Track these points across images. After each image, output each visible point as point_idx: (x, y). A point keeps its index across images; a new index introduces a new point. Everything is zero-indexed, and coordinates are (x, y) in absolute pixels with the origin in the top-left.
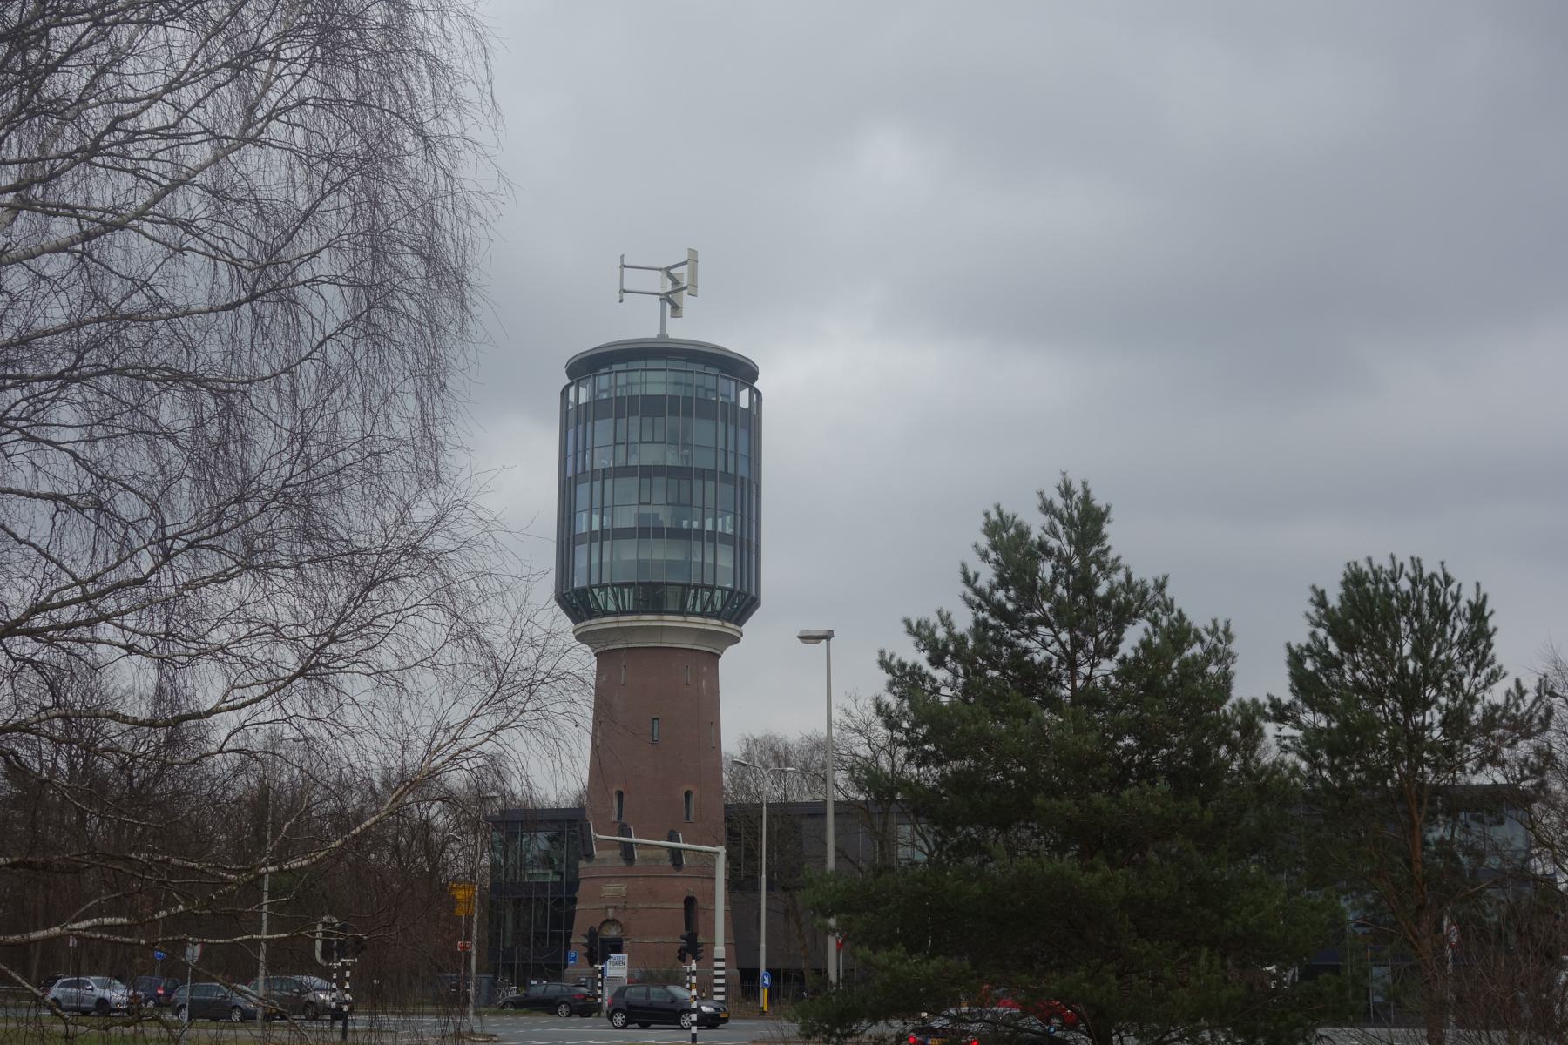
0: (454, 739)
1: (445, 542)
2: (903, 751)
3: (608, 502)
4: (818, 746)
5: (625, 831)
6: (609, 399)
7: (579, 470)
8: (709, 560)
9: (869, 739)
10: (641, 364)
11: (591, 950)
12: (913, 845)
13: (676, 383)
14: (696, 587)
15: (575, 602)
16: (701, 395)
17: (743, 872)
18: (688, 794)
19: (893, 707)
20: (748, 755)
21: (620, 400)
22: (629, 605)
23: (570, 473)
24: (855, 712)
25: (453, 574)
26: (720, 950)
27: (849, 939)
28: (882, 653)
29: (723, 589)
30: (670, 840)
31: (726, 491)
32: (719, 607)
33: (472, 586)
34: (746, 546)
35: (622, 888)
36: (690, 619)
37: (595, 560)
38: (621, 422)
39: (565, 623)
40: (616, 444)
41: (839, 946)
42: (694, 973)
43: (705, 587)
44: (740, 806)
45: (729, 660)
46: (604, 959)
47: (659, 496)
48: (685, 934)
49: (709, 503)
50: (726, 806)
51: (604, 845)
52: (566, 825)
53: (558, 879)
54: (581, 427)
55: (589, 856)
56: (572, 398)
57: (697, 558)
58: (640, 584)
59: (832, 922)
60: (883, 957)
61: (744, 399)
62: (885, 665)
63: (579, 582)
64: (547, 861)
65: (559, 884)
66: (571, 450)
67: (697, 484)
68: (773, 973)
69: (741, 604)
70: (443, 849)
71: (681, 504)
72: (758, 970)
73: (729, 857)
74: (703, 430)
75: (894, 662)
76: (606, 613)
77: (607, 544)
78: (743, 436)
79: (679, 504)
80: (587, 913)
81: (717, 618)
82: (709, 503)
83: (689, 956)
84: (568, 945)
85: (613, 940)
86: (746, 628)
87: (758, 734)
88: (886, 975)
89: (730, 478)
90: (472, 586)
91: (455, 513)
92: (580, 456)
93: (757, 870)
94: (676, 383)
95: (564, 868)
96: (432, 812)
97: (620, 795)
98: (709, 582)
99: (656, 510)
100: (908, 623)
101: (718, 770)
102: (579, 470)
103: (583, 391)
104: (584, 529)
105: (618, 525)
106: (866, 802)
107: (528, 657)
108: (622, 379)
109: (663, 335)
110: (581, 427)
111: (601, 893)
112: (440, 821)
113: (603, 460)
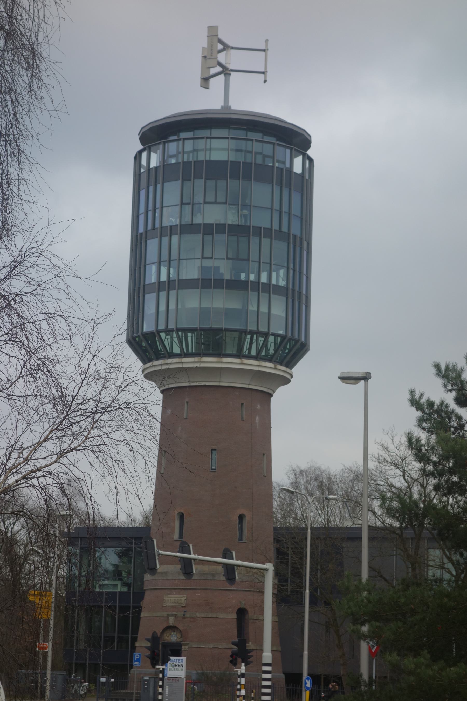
0: (26, 460)
1: (23, 284)
2: (433, 481)
3: (174, 255)
4: (357, 477)
5: (184, 548)
6: (177, 163)
7: (150, 227)
8: (264, 309)
9: (404, 472)
10: (206, 133)
11: (153, 652)
12: (442, 567)
13: (237, 150)
14: (252, 333)
15: (145, 345)
16: (259, 160)
17: (289, 588)
18: (241, 517)
19: (423, 442)
20: (295, 484)
21: (186, 164)
22: (192, 348)
23: (141, 229)
24: (391, 447)
25: (27, 315)
26: (267, 656)
27: (383, 648)
28: (412, 392)
29: (276, 335)
30: (225, 557)
31: (280, 247)
32: (272, 351)
33: (44, 325)
34: (297, 297)
35: (181, 599)
36: (246, 361)
37: (162, 308)
38: (188, 184)
39: (133, 364)
40: (182, 204)
41: (372, 655)
42: (243, 675)
43: (258, 333)
44: (288, 529)
45: (281, 399)
46: (165, 661)
47: (220, 252)
48: (236, 640)
49: (265, 258)
50: (275, 529)
51: (166, 560)
52: (133, 542)
53: (125, 589)
54: (151, 189)
55: (153, 570)
56: (144, 162)
57: (253, 307)
58: (201, 329)
59: (365, 629)
60: (409, 662)
61: (298, 166)
62: (415, 403)
63: (148, 326)
64: (117, 573)
65: (128, 593)
66: (142, 209)
67: (254, 241)
68: (315, 678)
69: (292, 349)
70: (25, 560)
71: (239, 259)
72: (301, 675)
73: (277, 574)
74: (261, 193)
75: (423, 400)
76: (171, 355)
77: (173, 293)
78: (296, 198)
79: (237, 259)
80: (151, 619)
81: (270, 361)
82: (265, 258)
83: (239, 660)
84: (134, 648)
85: (173, 644)
86: (297, 370)
87: (304, 466)
88: (412, 678)
89: (284, 236)
90: (44, 325)
91: (32, 259)
92: (150, 214)
93: (301, 587)
94: (237, 150)
95: (131, 580)
96: (17, 527)
97: (182, 516)
98: (263, 328)
99: (217, 263)
100: (437, 366)
101: (270, 496)
102: (150, 227)
103: (154, 157)
104: (153, 279)
105: (184, 276)
106: (400, 528)
107: (90, 390)
108: (189, 146)
109: (226, 107)
110: (151, 189)
111: (164, 603)
112: (22, 536)
113: (171, 218)
